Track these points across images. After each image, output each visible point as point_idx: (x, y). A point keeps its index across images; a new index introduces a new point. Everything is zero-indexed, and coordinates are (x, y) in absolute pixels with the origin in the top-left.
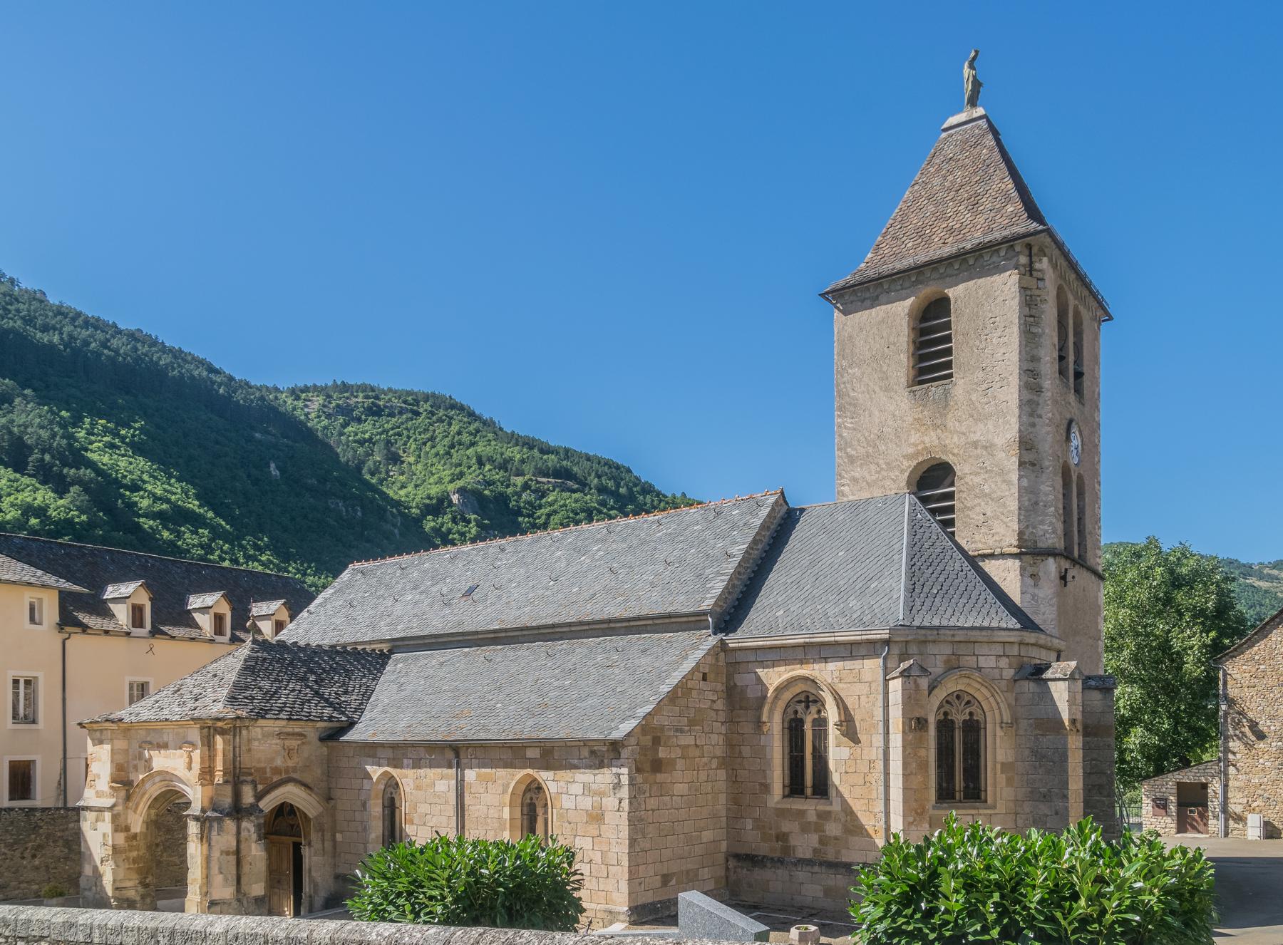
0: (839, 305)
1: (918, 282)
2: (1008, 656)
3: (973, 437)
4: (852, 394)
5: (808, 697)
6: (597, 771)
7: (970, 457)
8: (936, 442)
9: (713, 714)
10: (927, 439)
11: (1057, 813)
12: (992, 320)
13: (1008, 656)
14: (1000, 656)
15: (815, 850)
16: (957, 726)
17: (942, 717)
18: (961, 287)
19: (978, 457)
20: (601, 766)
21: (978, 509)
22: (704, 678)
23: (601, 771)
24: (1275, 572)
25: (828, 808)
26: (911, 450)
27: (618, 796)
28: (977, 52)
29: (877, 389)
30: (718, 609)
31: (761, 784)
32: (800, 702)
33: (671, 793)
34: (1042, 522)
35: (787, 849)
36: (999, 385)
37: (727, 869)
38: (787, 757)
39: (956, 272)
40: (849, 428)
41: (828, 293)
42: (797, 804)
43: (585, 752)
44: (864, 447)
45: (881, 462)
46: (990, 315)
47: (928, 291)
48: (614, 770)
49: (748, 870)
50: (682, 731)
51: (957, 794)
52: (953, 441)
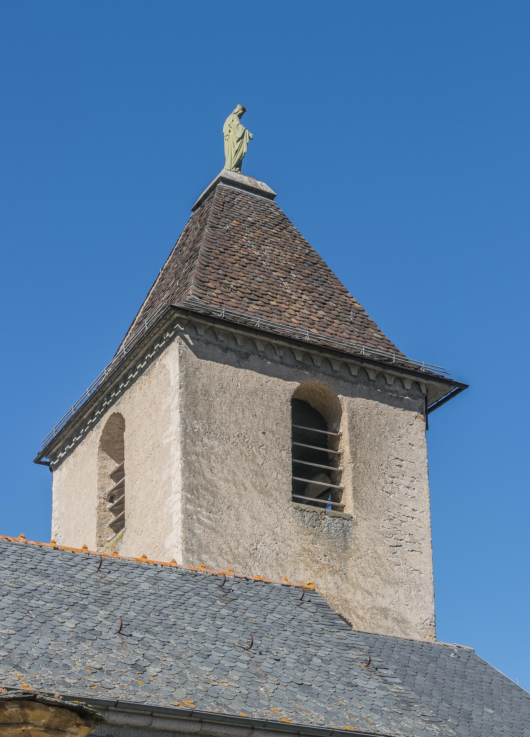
0: (187, 336)
3: (385, 603)
4: (208, 475)
8: (334, 592)
12: (398, 462)
18: (360, 401)
28: (244, 110)
29: (248, 484)
36: (410, 547)
39: (352, 379)
40: (206, 526)
44: (228, 562)
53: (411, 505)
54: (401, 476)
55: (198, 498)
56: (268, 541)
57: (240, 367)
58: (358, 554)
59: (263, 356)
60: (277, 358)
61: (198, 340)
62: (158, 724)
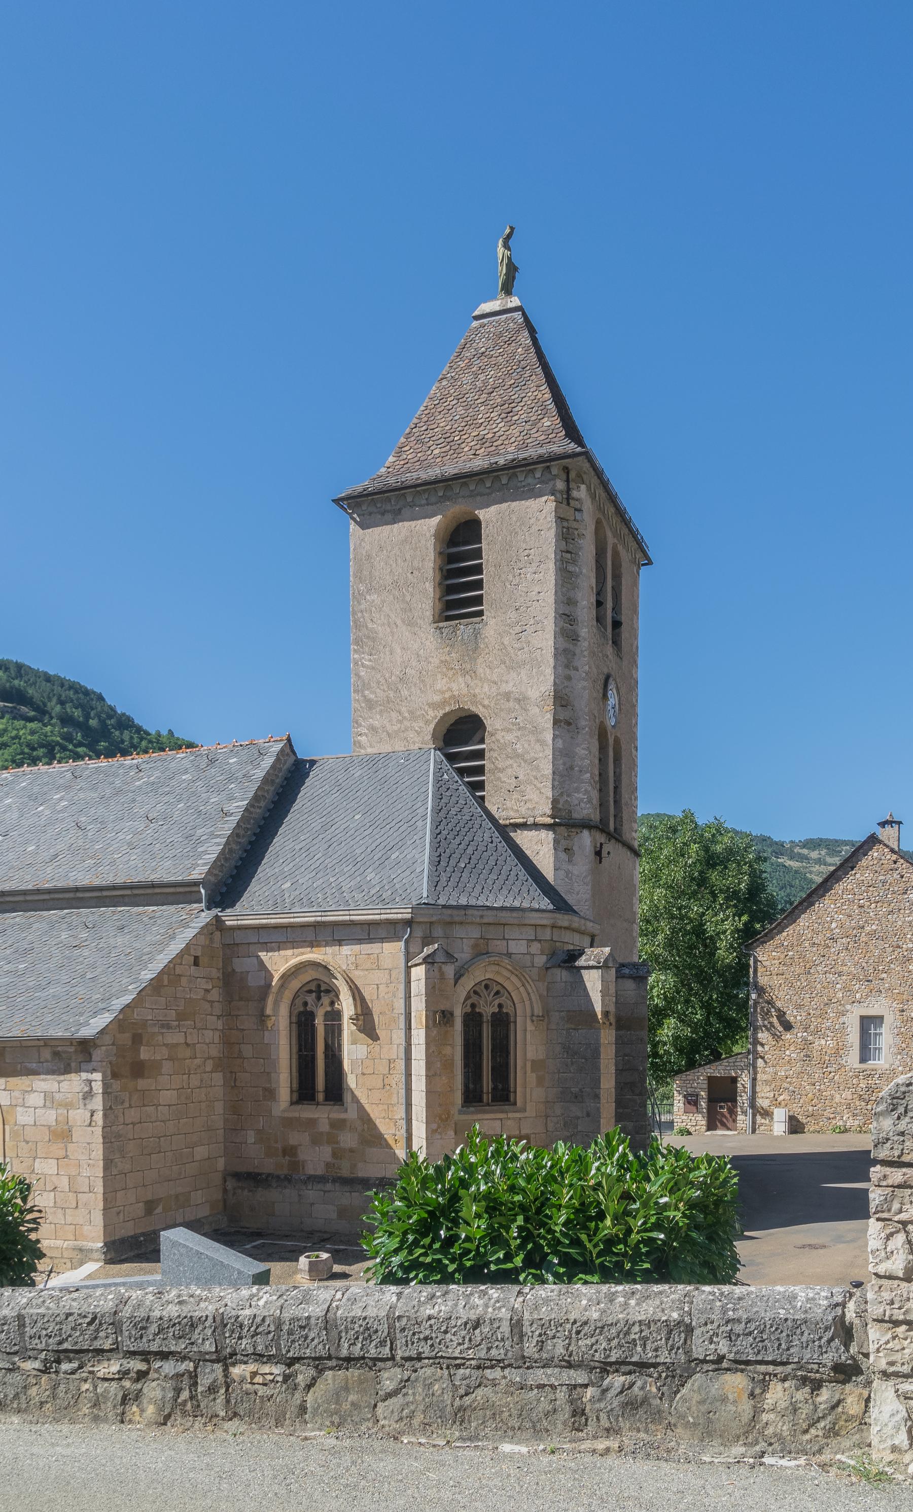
0: (355, 516)
1: (445, 498)
2: (540, 941)
3: (505, 688)
5: (319, 986)
6: (62, 1078)
7: (502, 710)
8: (465, 691)
9: (207, 1006)
10: (455, 686)
11: (588, 1115)
13: (540, 941)
14: (532, 940)
15: (328, 1165)
16: (485, 1019)
17: (469, 1009)
18: (493, 509)
19: (510, 711)
20: (67, 1070)
21: (509, 771)
22: (196, 963)
23: (67, 1077)
24: (805, 851)
25: (343, 1116)
26: (437, 698)
27: (89, 1107)
29: (399, 622)
30: (212, 879)
31: (265, 1089)
32: (310, 992)
33: (156, 1102)
34: (577, 790)
35: (296, 1165)
36: (533, 629)
37: (225, 1191)
38: (295, 1056)
39: (488, 491)
41: (342, 499)
42: (307, 1112)
43: (47, 1054)
44: (384, 691)
45: (404, 709)
46: (524, 546)
47: (457, 509)
48: (84, 1075)
49: (250, 1191)
50: (169, 1027)
51: (485, 1096)
52: (484, 691)
53: (537, 590)
54: (528, 565)
55: (362, 647)
56: (414, 664)
57: (395, 523)
58: (487, 651)
59: (412, 505)
60: (424, 502)
61: (363, 515)
62: (29, 898)
